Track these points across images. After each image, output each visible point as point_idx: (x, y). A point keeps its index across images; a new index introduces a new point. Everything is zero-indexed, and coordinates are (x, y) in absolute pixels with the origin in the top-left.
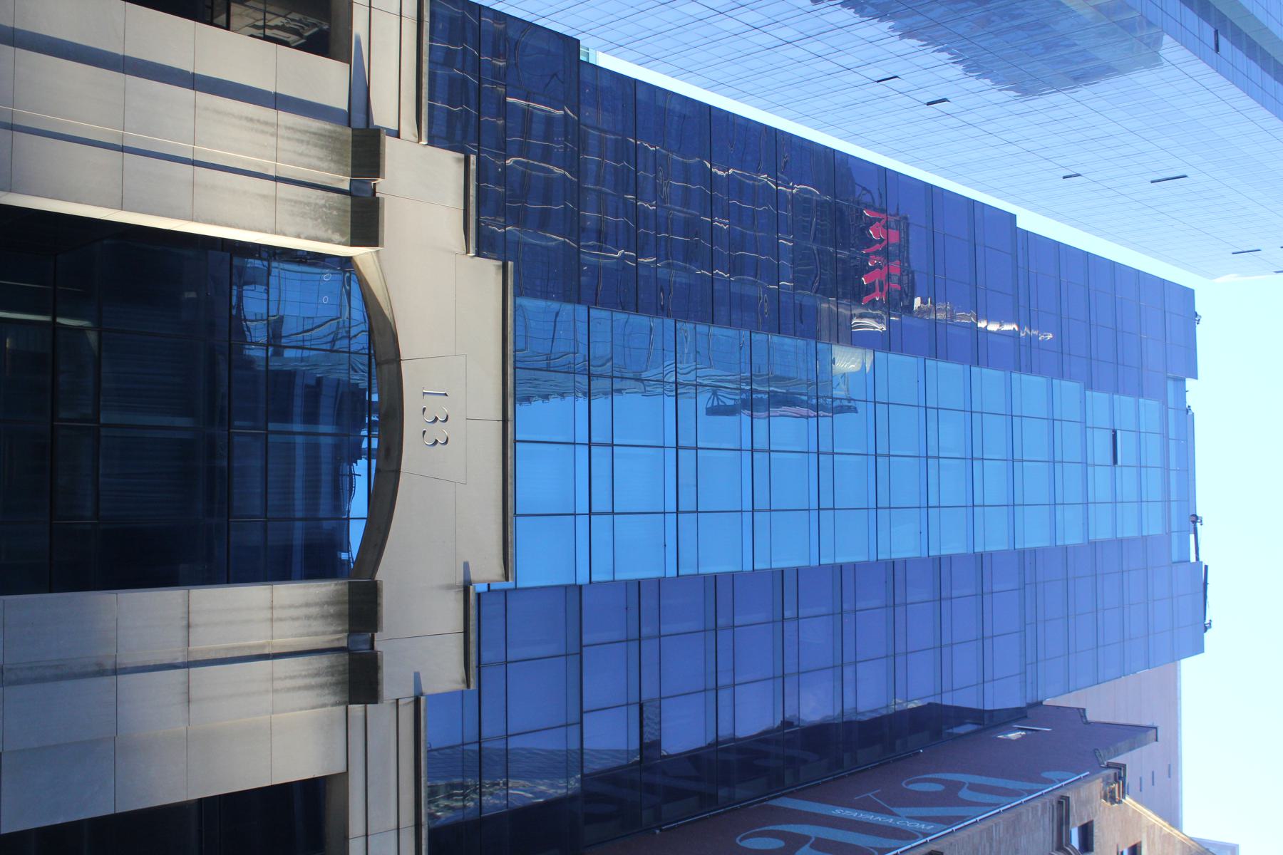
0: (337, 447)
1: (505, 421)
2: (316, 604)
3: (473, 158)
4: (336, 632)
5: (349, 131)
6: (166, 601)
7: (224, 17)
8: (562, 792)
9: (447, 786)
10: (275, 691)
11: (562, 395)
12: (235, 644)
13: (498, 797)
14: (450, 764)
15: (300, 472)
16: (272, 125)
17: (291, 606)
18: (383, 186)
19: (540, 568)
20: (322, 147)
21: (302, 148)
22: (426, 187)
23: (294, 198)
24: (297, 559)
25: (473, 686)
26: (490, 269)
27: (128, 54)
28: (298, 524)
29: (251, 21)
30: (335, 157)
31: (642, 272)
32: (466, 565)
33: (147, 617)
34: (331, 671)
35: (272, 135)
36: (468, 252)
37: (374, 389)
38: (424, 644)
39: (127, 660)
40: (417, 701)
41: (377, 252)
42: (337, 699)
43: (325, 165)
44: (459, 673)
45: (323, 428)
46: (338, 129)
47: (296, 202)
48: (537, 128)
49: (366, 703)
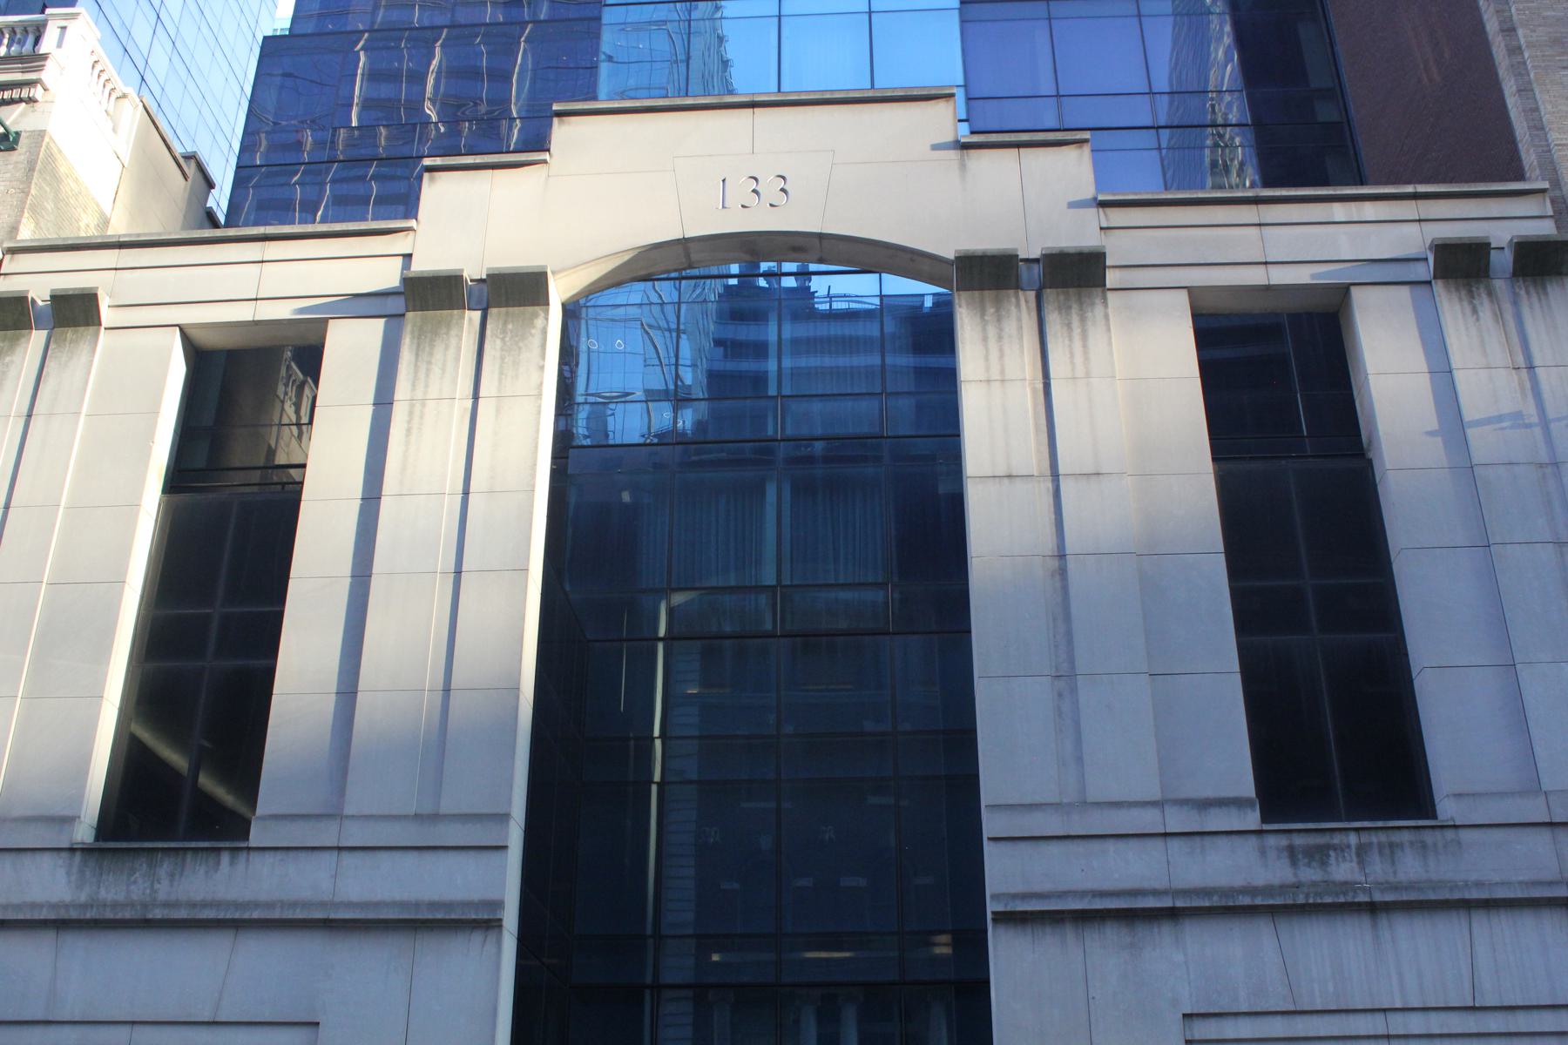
0: (795, 317)
1: (753, 105)
2: (984, 330)
3: (427, 162)
4: (1018, 305)
5: (410, 315)
6: (1015, 755)
7: (292, 471)
8: (1228, 28)
9: (1213, 174)
10: (1088, 375)
11: (721, 39)
12: (1031, 422)
13: (1229, 105)
14: (1183, 164)
15: (828, 361)
16: (412, 406)
17: (987, 358)
18: (473, 270)
19: (939, 54)
20: (432, 346)
21: (436, 370)
22: (468, 217)
23: (496, 376)
24: (933, 361)
25: (1087, 135)
26: (563, 133)
27: (349, 573)
28: (889, 360)
29: (294, 442)
30: (444, 330)
31: (523, 114)
32: (935, 147)
33: (1000, 525)
34: (1064, 309)
35: (424, 405)
36: (545, 162)
37: (723, 270)
38: (1034, 197)
39: (1048, 544)
40: (1104, 204)
41: (553, 273)
42: (1098, 301)
43: (453, 341)
44: (1070, 153)
45: (772, 336)
46: (408, 328)
47: (501, 373)
48: (385, 90)
49: (1105, 267)
